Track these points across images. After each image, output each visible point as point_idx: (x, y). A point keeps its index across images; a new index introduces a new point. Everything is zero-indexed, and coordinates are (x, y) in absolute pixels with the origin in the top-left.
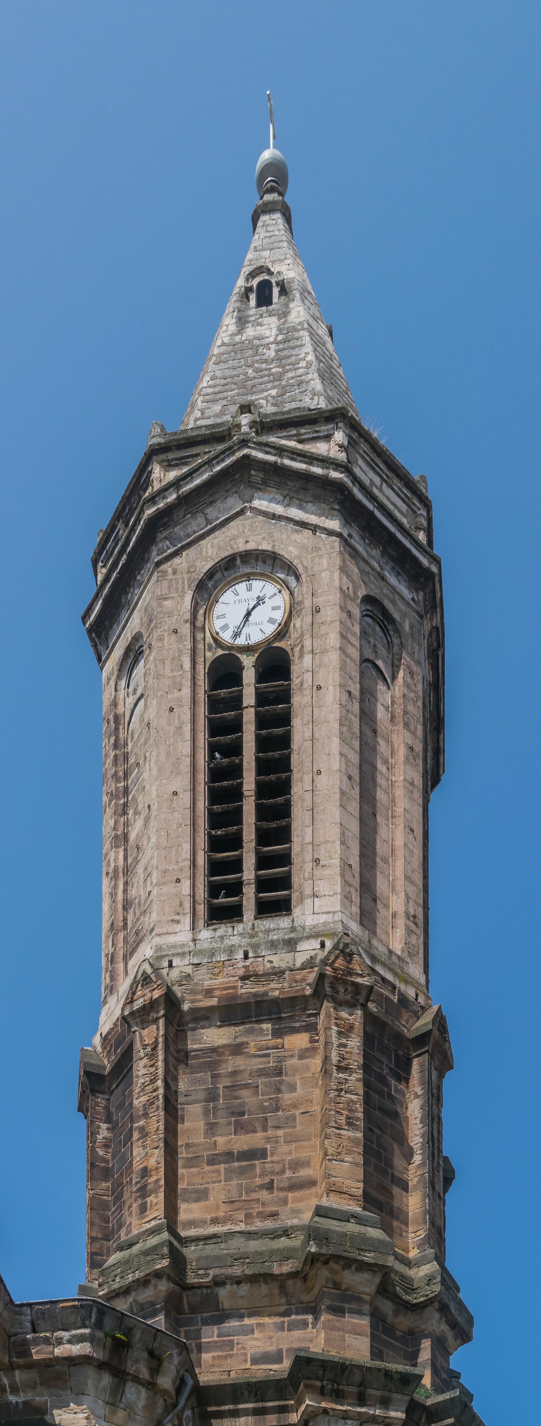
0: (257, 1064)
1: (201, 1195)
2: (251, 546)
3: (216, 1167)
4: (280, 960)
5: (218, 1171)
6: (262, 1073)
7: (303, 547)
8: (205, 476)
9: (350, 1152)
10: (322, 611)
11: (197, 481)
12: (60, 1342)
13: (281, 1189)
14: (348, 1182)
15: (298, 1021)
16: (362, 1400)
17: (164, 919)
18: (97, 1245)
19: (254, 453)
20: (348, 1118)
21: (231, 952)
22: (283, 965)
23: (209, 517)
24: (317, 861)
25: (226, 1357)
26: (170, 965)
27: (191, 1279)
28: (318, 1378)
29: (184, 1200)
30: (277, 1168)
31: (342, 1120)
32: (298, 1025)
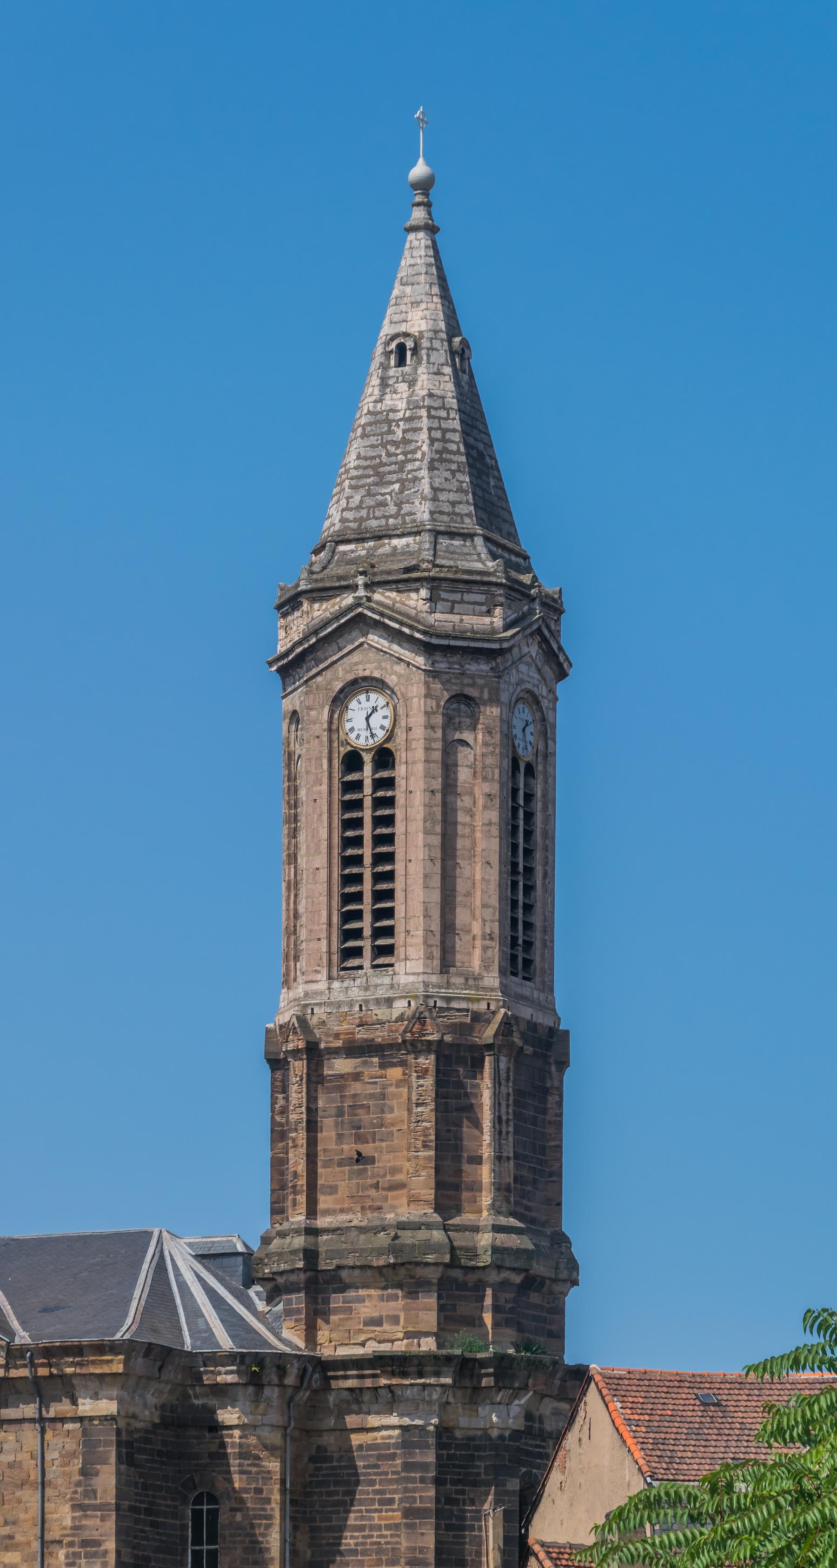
0: (370, 1090)
1: (333, 1190)
2: (367, 673)
3: (342, 1168)
4: (381, 1013)
5: (344, 1172)
6: (372, 1096)
7: (400, 676)
8: (335, 626)
9: (425, 1168)
10: (413, 729)
11: (329, 630)
12: (220, 1373)
13: (384, 1189)
14: (422, 1192)
15: (395, 1058)
16: (421, 1375)
17: (310, 969)
18: (275, 1195)
19: (366, 612)
20: (424, 1141)
21: (351, 1005)
22: (385, 1018)
23: (341, 645)
24: (408, 932)
25: (347, 1319)
26: (312, 1013)
27: (322, 1266)
28: (389, 1366)
29: (323, 1193)
30: (382, 1172)
31: (419, 1144)
32: (395, 1060)
